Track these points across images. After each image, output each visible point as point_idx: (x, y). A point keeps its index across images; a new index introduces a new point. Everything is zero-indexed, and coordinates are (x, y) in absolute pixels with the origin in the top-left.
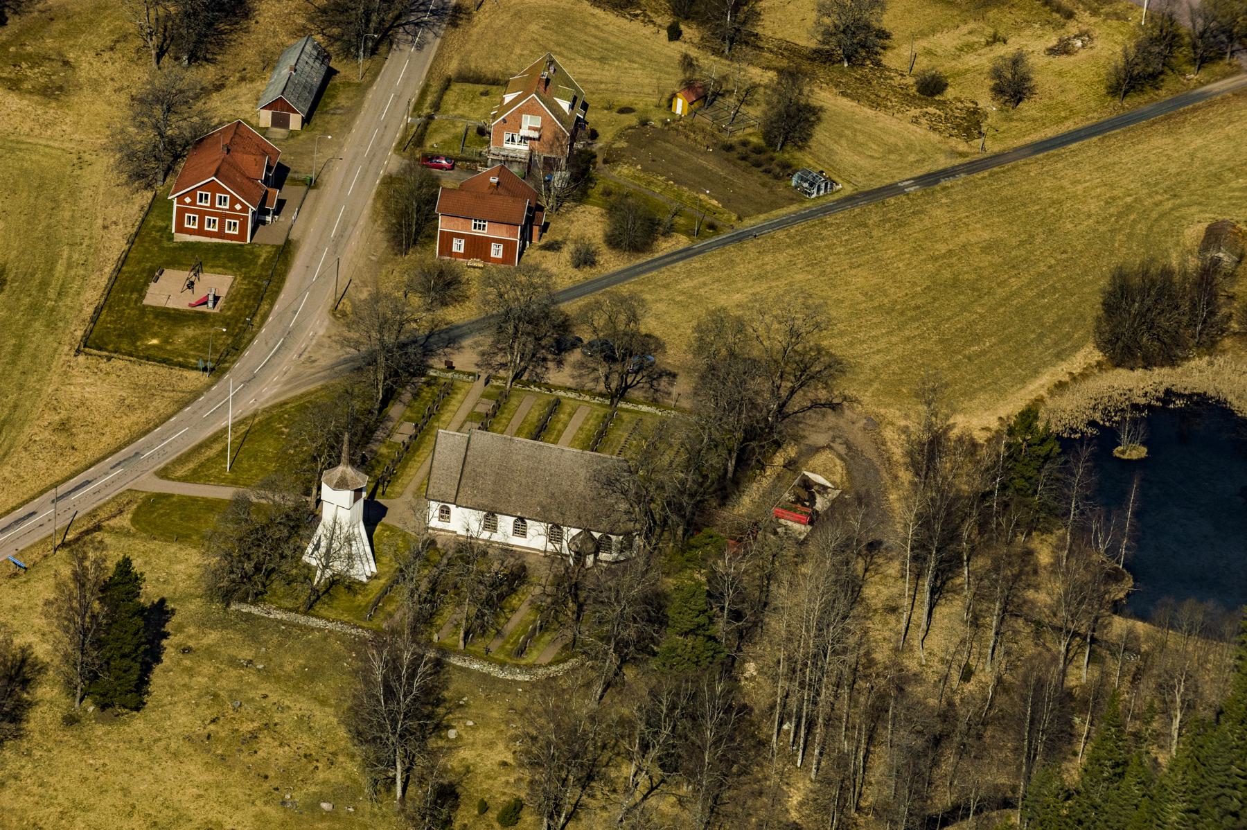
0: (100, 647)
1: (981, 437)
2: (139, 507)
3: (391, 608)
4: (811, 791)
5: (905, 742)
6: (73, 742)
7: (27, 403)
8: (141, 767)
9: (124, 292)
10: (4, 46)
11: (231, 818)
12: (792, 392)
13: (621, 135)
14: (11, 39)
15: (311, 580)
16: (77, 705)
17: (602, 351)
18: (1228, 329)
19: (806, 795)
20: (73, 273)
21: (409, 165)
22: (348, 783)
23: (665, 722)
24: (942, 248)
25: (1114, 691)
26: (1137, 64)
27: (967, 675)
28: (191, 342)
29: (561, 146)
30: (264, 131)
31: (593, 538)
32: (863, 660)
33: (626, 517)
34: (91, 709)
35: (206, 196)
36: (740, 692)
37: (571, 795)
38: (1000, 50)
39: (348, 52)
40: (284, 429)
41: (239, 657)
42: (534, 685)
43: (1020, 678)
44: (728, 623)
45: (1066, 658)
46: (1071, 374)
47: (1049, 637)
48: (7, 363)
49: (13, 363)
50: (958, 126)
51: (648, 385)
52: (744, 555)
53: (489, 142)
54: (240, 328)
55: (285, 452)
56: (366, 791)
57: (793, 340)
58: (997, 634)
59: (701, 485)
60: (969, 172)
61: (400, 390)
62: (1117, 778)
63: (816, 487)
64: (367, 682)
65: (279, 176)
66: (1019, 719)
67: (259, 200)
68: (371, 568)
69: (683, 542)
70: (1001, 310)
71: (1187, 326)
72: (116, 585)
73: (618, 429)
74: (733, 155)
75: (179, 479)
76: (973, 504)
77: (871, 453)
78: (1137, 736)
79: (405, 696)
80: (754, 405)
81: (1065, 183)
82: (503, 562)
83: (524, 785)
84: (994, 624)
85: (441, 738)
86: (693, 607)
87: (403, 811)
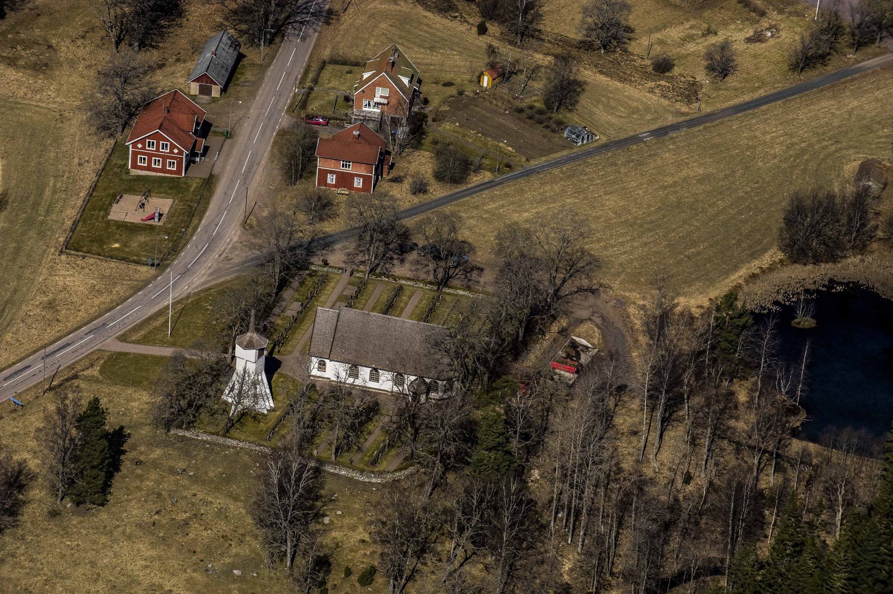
0: (77, 461)
1: (696, 312)
2: (105, 362)
3: (284, 432)
4: (578, 561)
5: (644, 527)
6: (56, 529)
7: (24, 289)
8: (104, 546)
9: (94, 210)
10: (4, 34)
11: (169, 581)
12: (564, 281)
13: (444, 102)
14: (9, 29)
15: (228, 413)
16: (58, 502)
17: (432, 252)
18: (875, 236)
19: (574, 563)
20: (57, 197)
21: (296, 123)
22: (253, 555)
23: (476, 511)
24: (670, 180)
25: (794, 492)
26: (811, 48)
27: (688, 479)
28: (144, 246)
29: (403, 109)
30: (194, 97)
31: (425, 383)
32: (614, 469)
33: (449, 368)
34: (69, 505)
35: (153, 143)
36: (528, 491)
37: (410, 563)
38: (713, 40)
39: (253, 42)
40: (209, 307)
41: (176, 467)
42: (384, 486)
43: (726, 482)
44: (519, 442)
45: (758, 468)
46: (761, 268)
47: (746, 454)
48: (10, 260)
49: (14, 260)
50: (682, 94)
51: (464, 276)
52: (531, 395)
53: (352, 106)
54: (178, 236)
55: (209, 323)
56: (265, 561)
57: (565, 245)
58: (709, 450)
59: (500, 345)
60: (689, 127)
61: (291, 280)
62: (796, 555)
63: (581, 348)
64: (267, 484)
65: (205, 129)
66: (726, 511)
67: (191, 147)
68: (271, 404)
69: (487, 385)
70: (711, 224)
71: (845, 235)
72: (89, 417)
73: (443, 307)
74: (524, 115)
75: (134, 342)
76: (691, 359)
77: (619, 325)
78: (811, 524)
79: (294, 494)
80: (537, 290)
81: (758, 134)
82: (363, 399)
83: (377, 556)
84: (707, 444)
85: (319, 523)
86: (495, 431)
87: (292, 575)
